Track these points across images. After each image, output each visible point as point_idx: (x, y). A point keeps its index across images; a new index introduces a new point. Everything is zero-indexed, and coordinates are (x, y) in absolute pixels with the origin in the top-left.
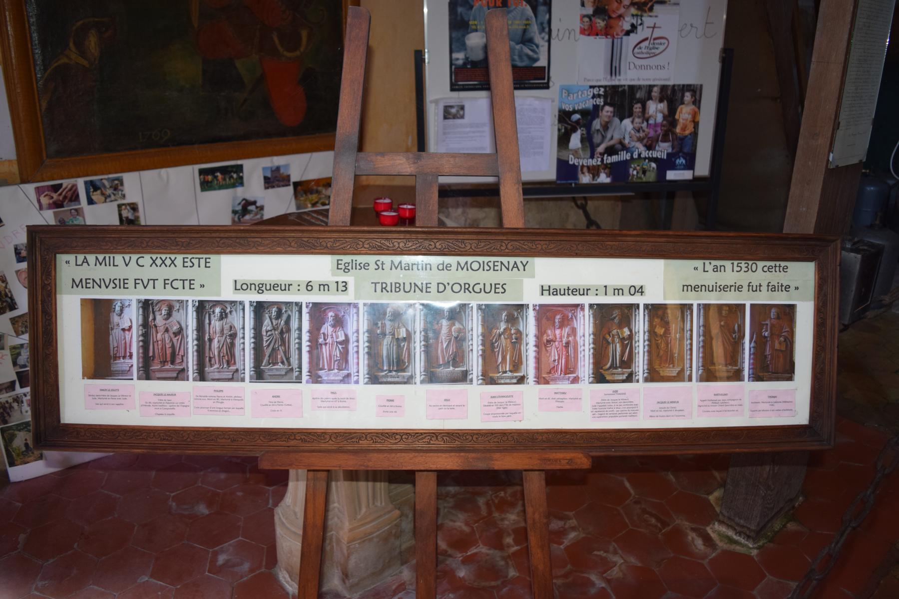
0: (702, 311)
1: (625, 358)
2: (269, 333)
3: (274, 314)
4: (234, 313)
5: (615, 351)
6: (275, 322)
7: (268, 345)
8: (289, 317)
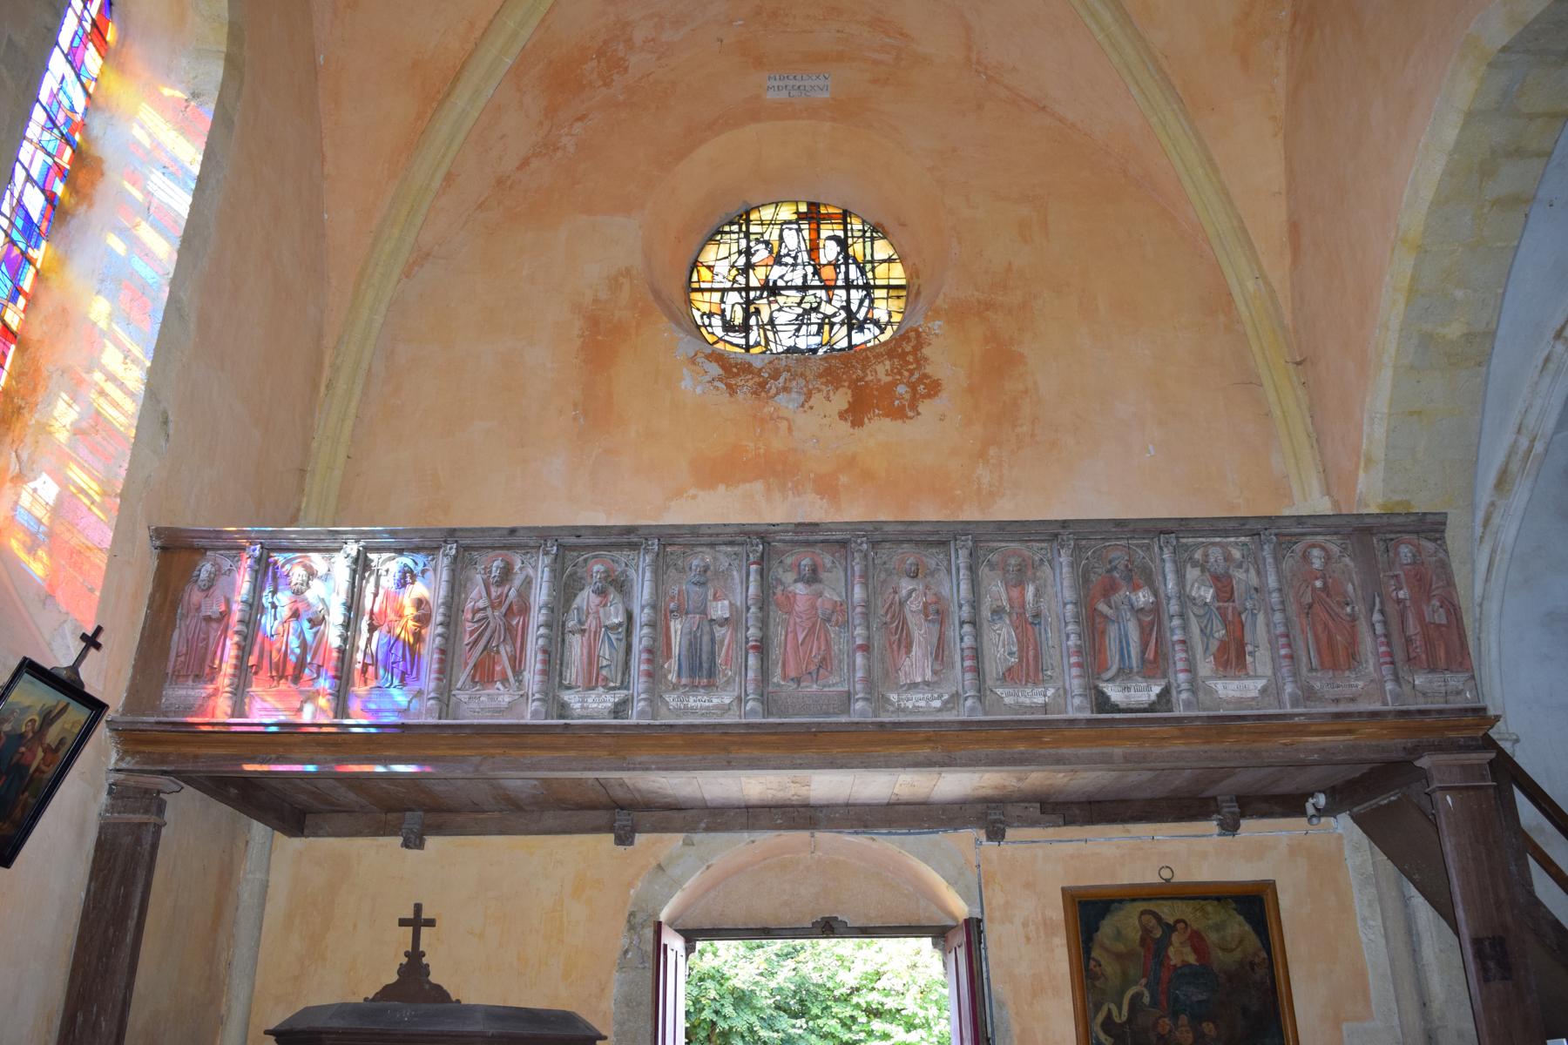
0: (1065, 751)
1: (1150, 654)
2: (478, 616)
3: (495, 573)
4: (430, 574)
5: (1124, 639)
6: (494, 592)
7: (476, 642)
8: (528, 582)
